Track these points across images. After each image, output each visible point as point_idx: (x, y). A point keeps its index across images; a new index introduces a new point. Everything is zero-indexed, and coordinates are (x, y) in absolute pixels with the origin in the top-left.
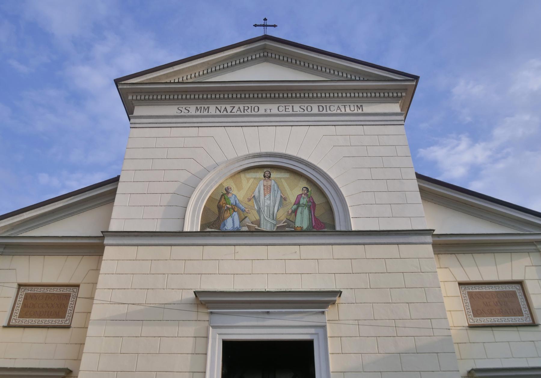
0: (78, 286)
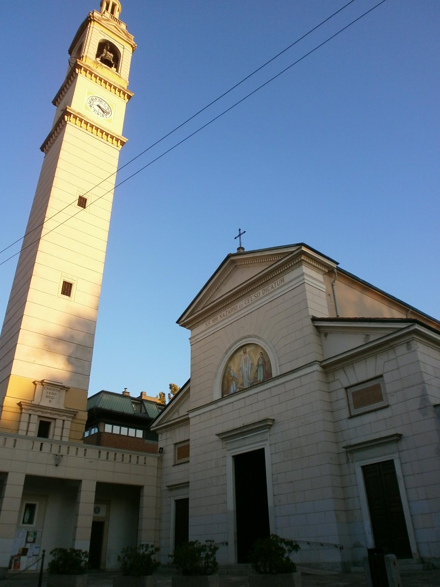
0: (381, 376)
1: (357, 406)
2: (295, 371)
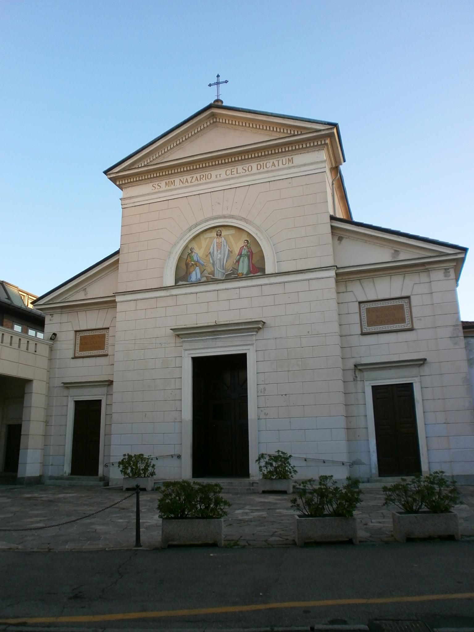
1: (370, 324)
2: (302, 271)
